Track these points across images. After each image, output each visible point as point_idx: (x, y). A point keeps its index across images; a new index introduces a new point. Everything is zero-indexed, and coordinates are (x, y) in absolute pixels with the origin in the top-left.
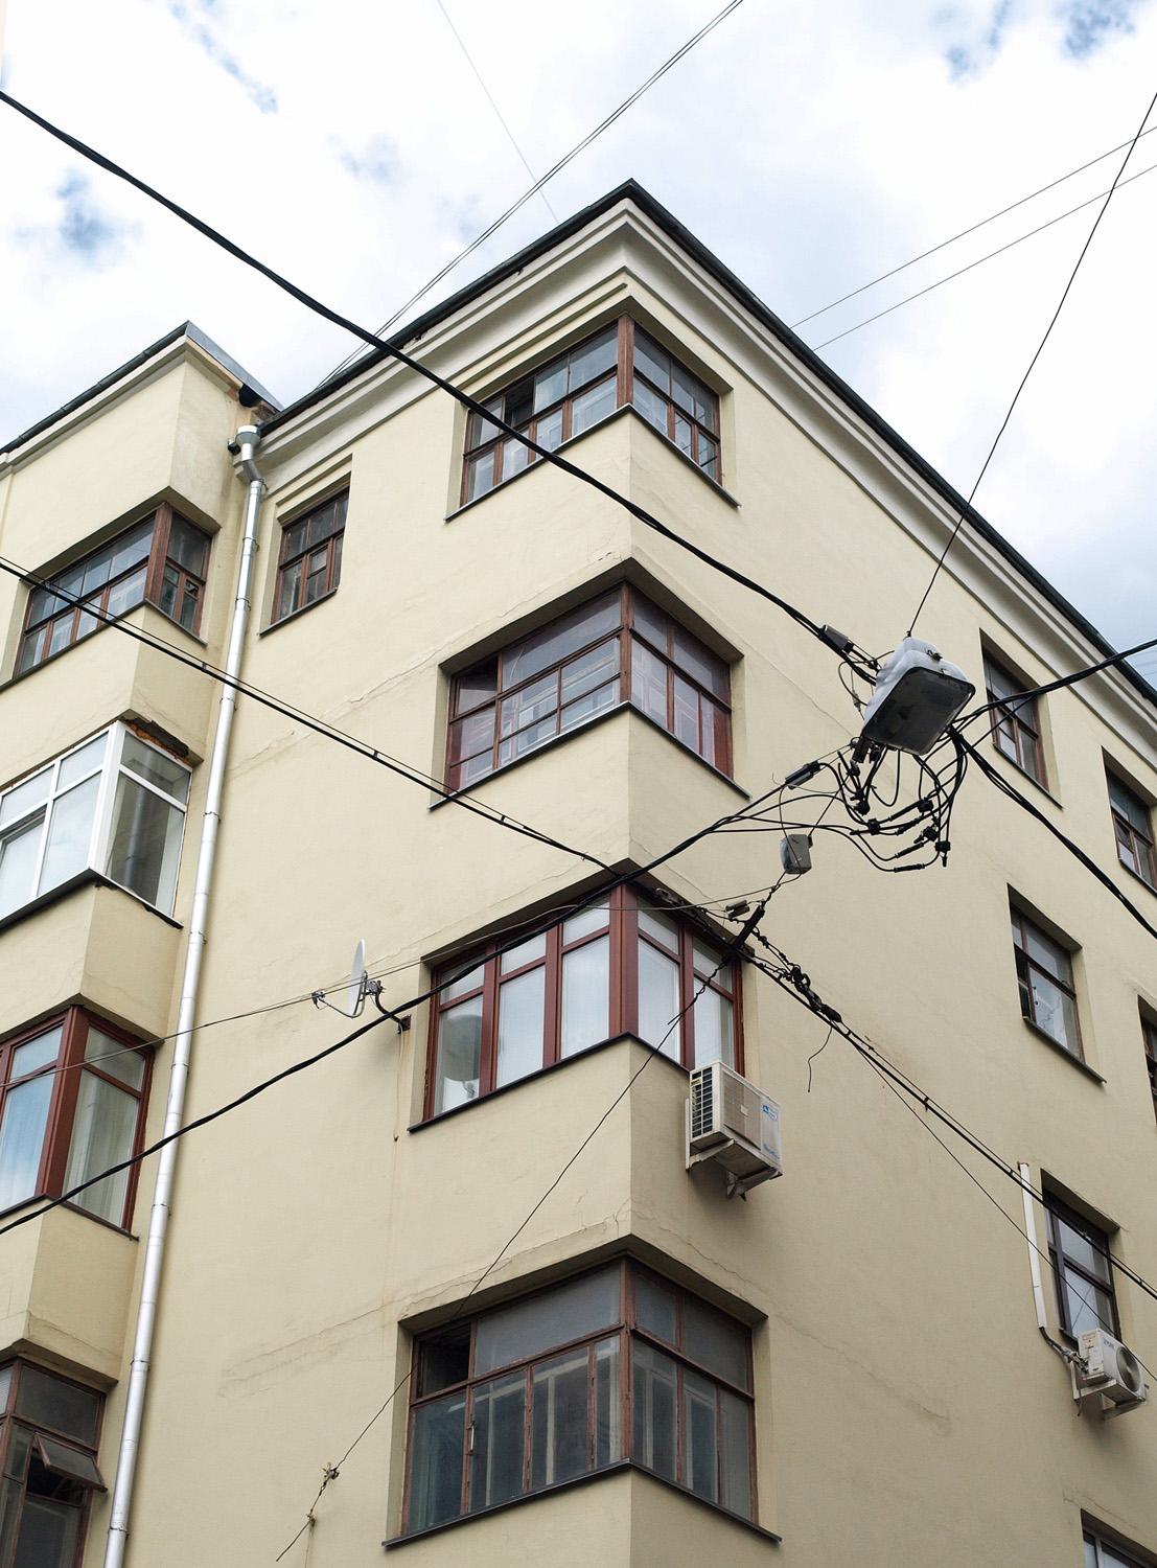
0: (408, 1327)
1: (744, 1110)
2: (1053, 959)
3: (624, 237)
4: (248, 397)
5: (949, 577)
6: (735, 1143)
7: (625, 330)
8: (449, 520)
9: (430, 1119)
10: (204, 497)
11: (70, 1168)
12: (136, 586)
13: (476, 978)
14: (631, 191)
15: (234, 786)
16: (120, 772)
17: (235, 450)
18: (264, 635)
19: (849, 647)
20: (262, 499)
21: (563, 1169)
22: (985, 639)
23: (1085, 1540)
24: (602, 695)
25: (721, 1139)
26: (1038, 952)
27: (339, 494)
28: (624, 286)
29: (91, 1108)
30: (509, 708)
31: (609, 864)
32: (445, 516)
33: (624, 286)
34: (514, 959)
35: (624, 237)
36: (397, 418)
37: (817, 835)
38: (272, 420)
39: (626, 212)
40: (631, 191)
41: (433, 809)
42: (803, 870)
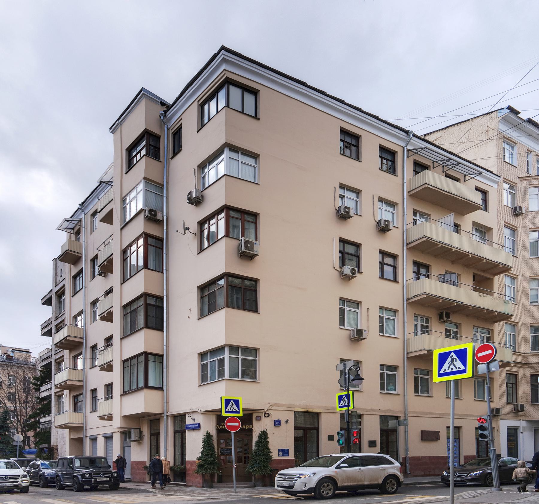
0: (259, 214)
1: (249, 245)
2: (112, 160)
3: (224, 60)
4: (163, 104)
5: (72, 308)
6: (491, 473)
7: (226, 151)
8: (198, 132)
9: (201, 250)
10: (155, 130)
11: (259, 371)
12: (144, 152)
13: (214, 221)
14: (223, 48)
15: (402, 356)
16: (344, 132)
17: (160, 117)
18: (126, 173)
19: (446, 176)
20: (168, 129)
21: (218, 261)
22: (91, 234)
23: (204, 439)
24: (402, 387)
25: (244, 252)
26: (348, 140)
27: (180, 128)
28: (225, 74)
29: (142, 247)
30: (343, 481)
31: (103, 345)
32: (119, 228)
33: (225, 74)
34: (212, 222)
35: (224, 60)
36: (105, 204)
37: (400, 285)
38: (166, 107)
39: (223, 54)
40: (223, 48)
41: (112, 254)
42: (199, 425)
